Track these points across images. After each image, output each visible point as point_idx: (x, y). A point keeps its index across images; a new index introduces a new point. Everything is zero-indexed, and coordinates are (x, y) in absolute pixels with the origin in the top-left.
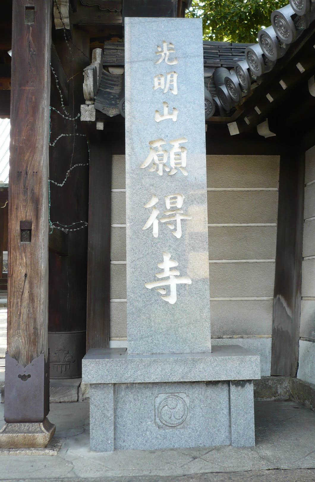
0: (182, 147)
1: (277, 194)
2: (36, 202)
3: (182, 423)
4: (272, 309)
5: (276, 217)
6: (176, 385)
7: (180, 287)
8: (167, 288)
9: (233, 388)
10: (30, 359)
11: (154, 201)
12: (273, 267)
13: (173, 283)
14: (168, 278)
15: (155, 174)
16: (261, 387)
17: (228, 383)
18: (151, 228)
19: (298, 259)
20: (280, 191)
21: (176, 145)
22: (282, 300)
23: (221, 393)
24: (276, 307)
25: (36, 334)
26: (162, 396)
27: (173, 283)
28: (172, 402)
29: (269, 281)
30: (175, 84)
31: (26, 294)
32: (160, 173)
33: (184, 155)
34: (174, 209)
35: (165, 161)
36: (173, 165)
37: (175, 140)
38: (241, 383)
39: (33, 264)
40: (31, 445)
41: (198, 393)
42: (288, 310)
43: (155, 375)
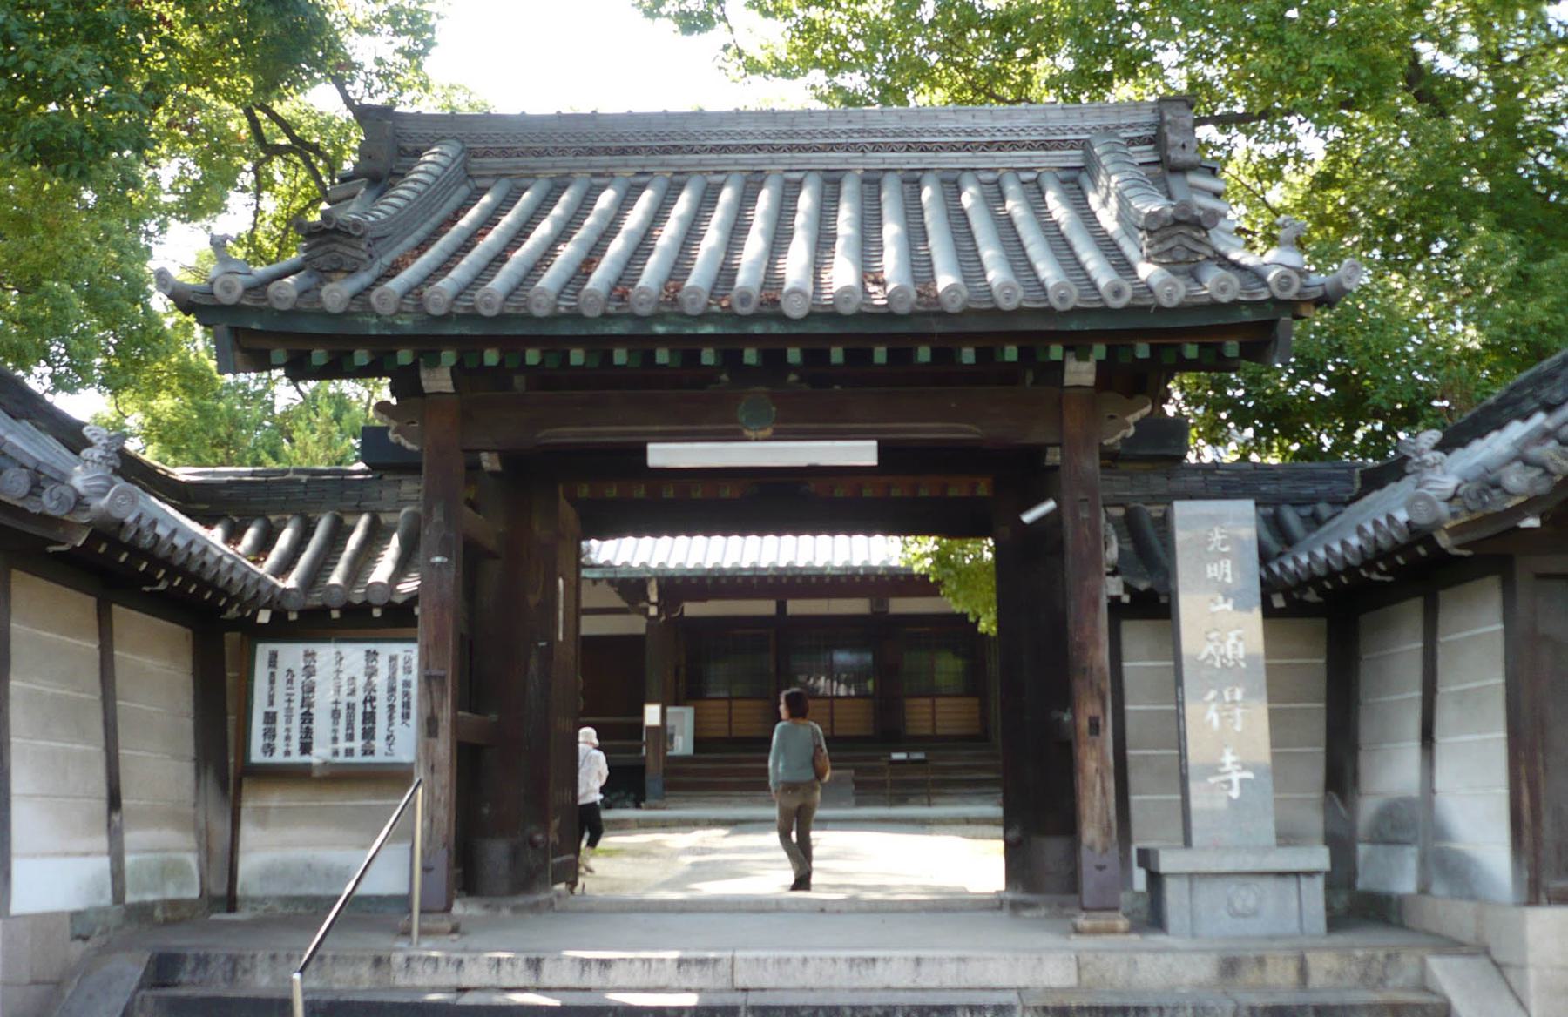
0: (1239, 638)
1: (1324, 668)
2: (1103, 699)
3: (1255, 913)
4: (95, 623)
5: (1324, 695)
6: (1239, 879)
7: (1242, 782)
8: (1229, 782)
9: (1303, 880)
10: (1105, 850)
11: (1212, 694)
12: (1322, 759)
13: (1235, 777)
14: (1229, 772)
15: (1212, 666)
16: (1327, 874)
17: (1297, 874)
18: (1211, 722)
19: (1354, 749)
20: (1329, 663)
21: (1232, 635)
22: (1335, 796)
23: (1291, 884)
24: (1328, 806)
25: (1109, 827)
26: (1234, 887)
27: (1235, 777)
28: (1243, 892)
29: (1319, 774)
30: (1229, 571)
31: (1098, 788)
32: (1218, 665)
33: (1241, 645)
34: (1233, 702)
35: (1222, 651)
36: (1230, 656)
37: (1232, 630)
38: (1310, 874)
39: (1102, 759)
40: (1112, 931)
41: (1269, 884)
42: (1342, 809)
43: (1228, 865)
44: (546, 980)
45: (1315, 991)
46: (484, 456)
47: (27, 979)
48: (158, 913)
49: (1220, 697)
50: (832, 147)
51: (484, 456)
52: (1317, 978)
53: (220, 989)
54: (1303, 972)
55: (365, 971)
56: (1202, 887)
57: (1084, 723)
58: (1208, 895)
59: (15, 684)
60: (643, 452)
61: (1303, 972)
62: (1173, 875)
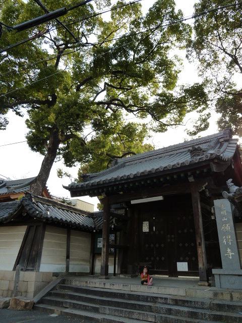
27: (230, 254)
44: (106, 287)
45: (234, 301)
46: (193, 180)
47: (41, 281)
48: (77, 274)
49: (226, 238)
50: (172, 151)
51: (193, 180)
52: (235, 299)
53: (69, 285)
54: (232, 297)
55: (85, 283)
56: (222, 277)
57: (198, 243)
58: (224, 279)
59: (45, 240)
60: (130, 202)
61: (232, 297)
62: (216, 274)
